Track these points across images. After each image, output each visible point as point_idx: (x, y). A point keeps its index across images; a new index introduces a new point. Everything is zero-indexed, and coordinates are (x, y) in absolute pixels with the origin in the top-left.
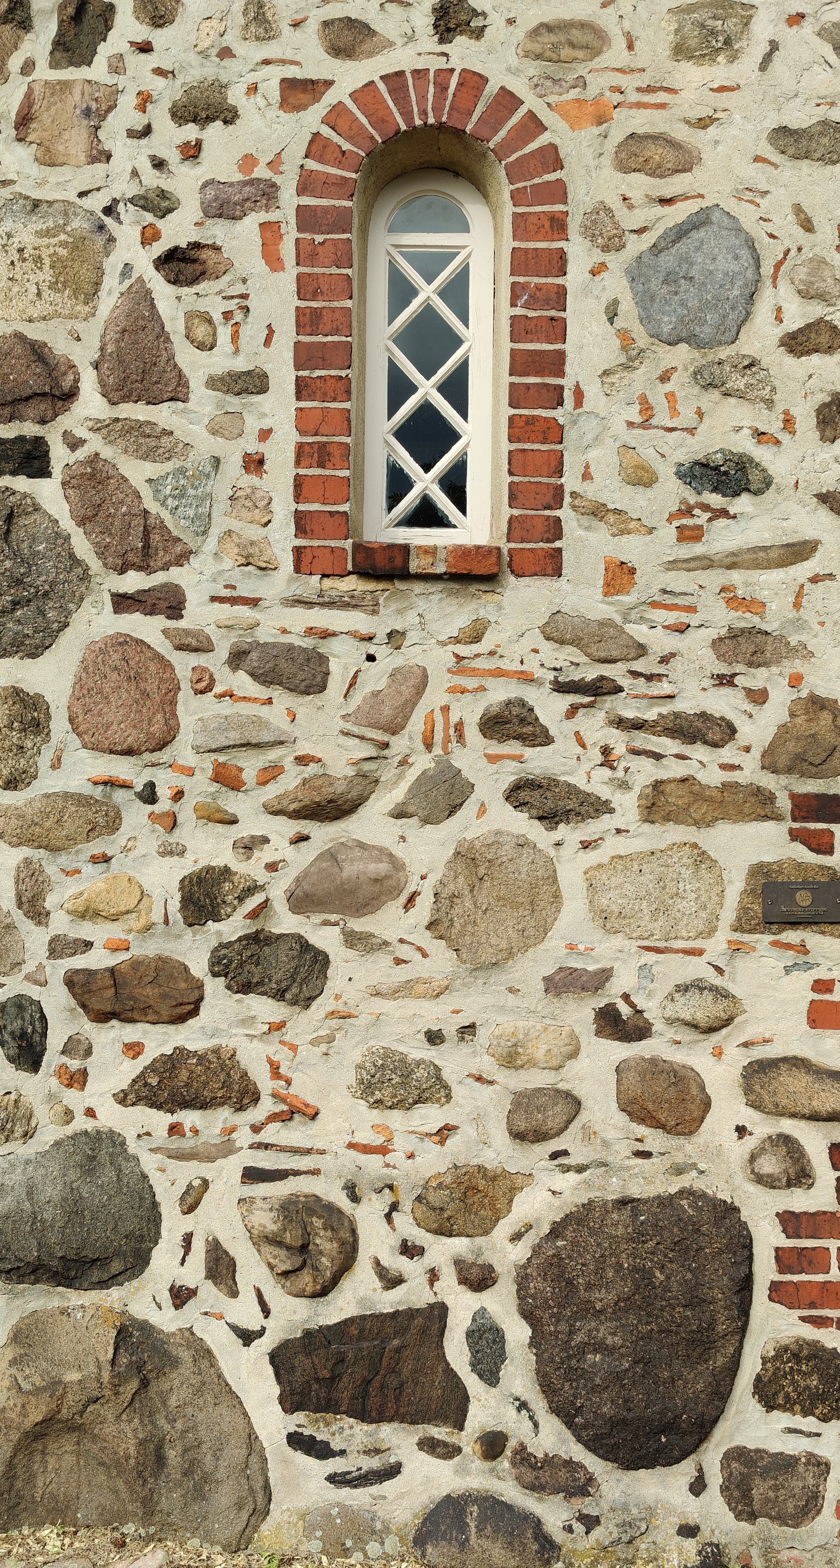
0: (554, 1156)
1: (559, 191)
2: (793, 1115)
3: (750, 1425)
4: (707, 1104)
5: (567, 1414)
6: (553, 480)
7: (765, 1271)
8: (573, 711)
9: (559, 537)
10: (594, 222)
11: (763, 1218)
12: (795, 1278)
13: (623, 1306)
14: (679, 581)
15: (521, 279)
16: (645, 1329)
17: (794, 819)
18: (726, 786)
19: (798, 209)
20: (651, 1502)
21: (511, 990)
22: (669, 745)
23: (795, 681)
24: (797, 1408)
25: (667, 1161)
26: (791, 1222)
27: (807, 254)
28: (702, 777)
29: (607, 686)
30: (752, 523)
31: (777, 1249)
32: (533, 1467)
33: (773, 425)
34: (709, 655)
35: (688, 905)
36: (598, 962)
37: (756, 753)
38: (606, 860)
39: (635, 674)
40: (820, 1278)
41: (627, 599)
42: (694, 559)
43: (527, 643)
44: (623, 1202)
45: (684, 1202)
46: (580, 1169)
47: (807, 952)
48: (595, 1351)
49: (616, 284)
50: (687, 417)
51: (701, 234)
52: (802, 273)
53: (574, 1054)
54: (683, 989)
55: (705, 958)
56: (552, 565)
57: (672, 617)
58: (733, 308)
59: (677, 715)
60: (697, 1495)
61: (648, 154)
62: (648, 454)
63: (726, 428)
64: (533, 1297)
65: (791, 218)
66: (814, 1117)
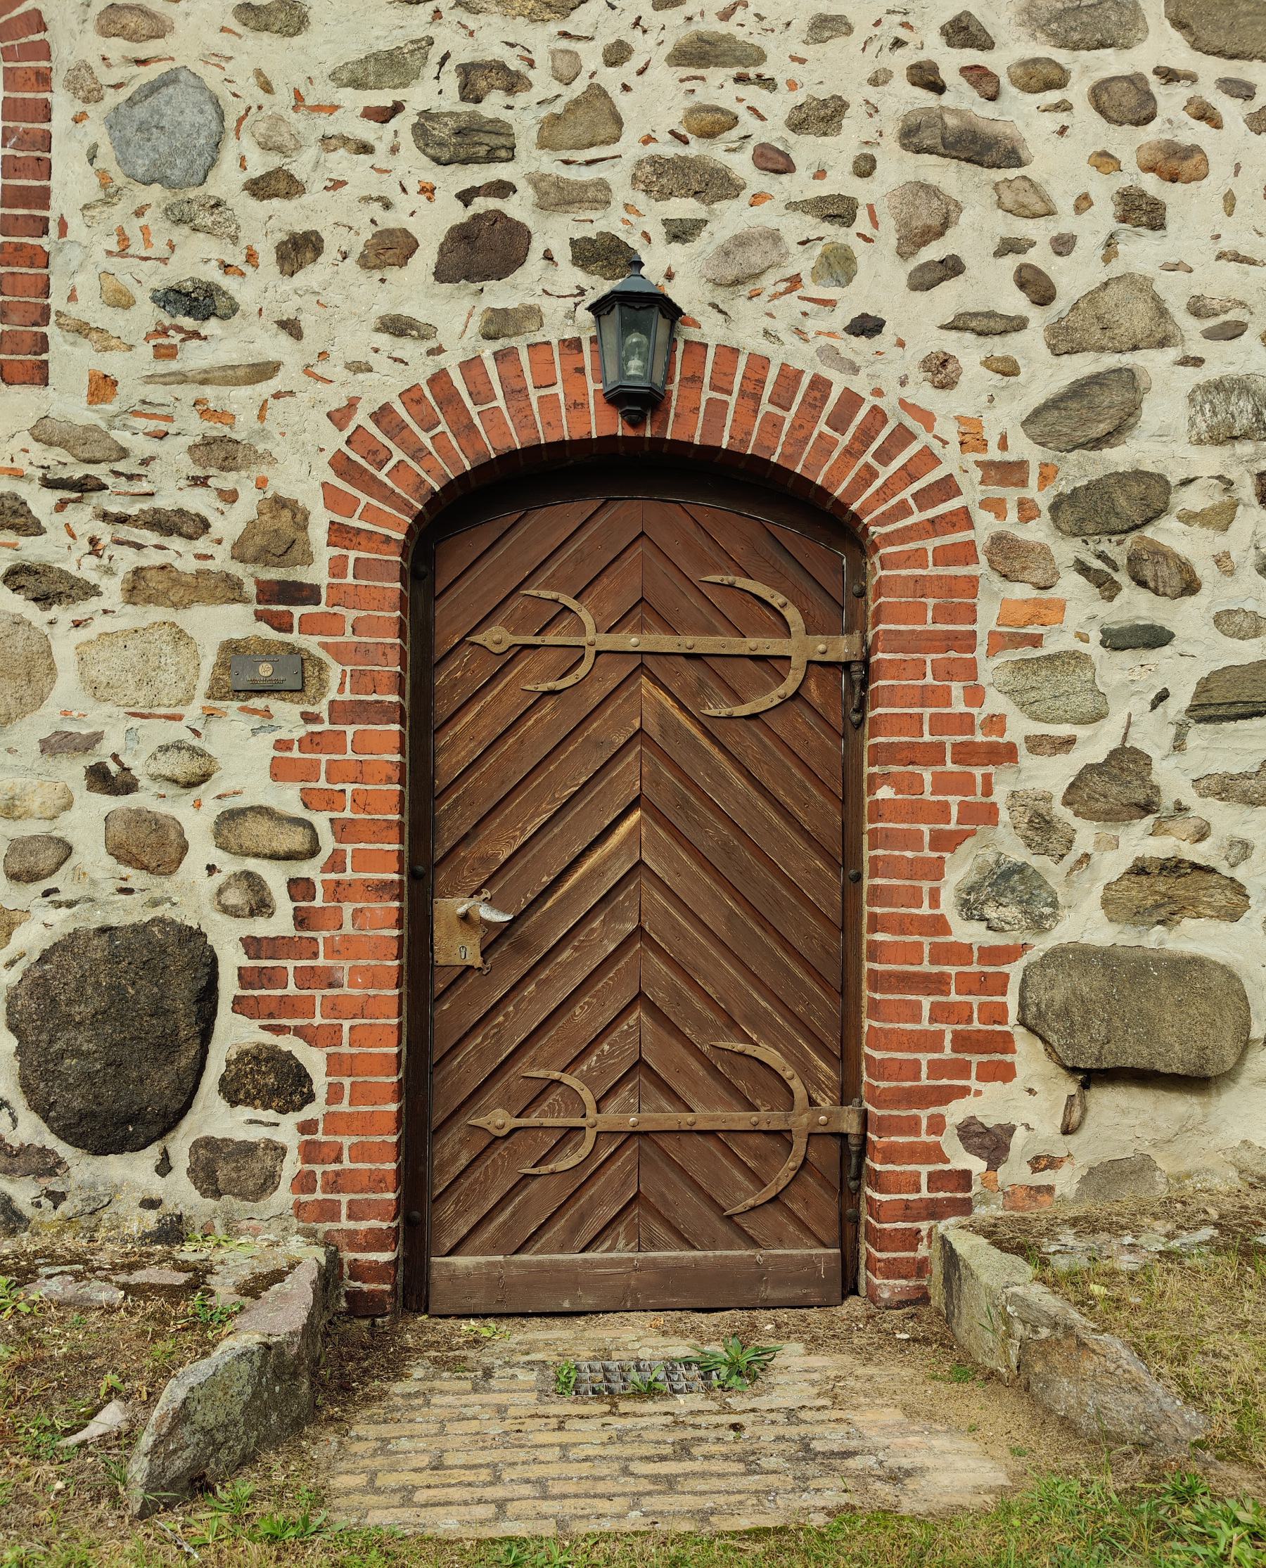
0: (47, 894)
1: (44, 51)
2: (257, 855)
3: (215, 1117)
4: (184, 848)
5: (43, 1109)
6: (39, 300)
7: (228, 986)
8: (61, 505)
9: (46, 350)
10: (76, 77)
11: (228, 943)
12: (256, 993)
13: (99, 1017)
14: (157, 393)
15: (11, 124)
16: (117, 1037)
17: (259, 602)
18: (199, 573)
19: (259, 73)
20: (117, 1182)
21: (9, 750)
22: (149, 537)
23: (261, 484)
24: (258, 1102)
25: (146, 897)
26: (252, 946)
27: (267, 111)
28: (178, 564)
29: (91, 484)
30: (221, 345)
31: (240, 969)
32: (10, 1155)
33: (236, 257)
34: (186, 459)
35: (169, 677)
36: (90, 726)
37: (227, 545)
38: (94, 637)
39: (117, 474)
40: (279, 992)
41: (111, 408)
42: (169, 374)
43: (17, 444)
44: (103, 930)
45: (155, 929)
46: (70, 905)
47: (271, 717)
48: (73, 1056)
49: (95, 131)
50: (160, 248)
51: (171, 90)
52: (262, 128)
53: (68, 806)
54: (164, 749)
55: (185, 722)
56: (40, 375)
57: (153, 425)
58: (200, 155)
59: (156, 511)
60: (163, 1175)
61: (124, 21)
62: (127, 281)
63: (196, 260)
64: (20, 1013)
65: (253, 80)
66: (274, 857)
